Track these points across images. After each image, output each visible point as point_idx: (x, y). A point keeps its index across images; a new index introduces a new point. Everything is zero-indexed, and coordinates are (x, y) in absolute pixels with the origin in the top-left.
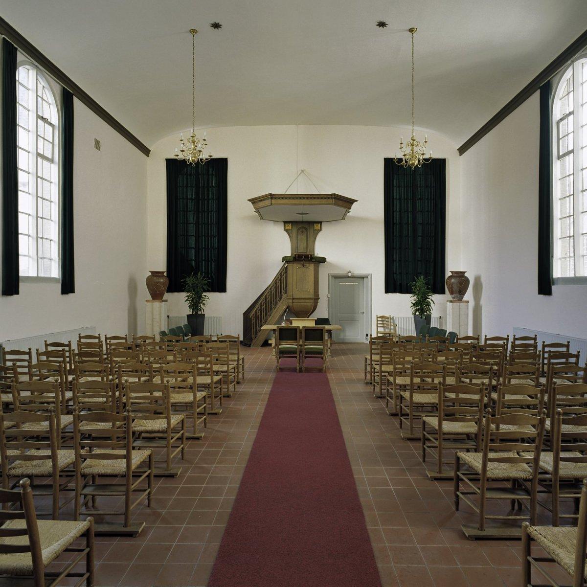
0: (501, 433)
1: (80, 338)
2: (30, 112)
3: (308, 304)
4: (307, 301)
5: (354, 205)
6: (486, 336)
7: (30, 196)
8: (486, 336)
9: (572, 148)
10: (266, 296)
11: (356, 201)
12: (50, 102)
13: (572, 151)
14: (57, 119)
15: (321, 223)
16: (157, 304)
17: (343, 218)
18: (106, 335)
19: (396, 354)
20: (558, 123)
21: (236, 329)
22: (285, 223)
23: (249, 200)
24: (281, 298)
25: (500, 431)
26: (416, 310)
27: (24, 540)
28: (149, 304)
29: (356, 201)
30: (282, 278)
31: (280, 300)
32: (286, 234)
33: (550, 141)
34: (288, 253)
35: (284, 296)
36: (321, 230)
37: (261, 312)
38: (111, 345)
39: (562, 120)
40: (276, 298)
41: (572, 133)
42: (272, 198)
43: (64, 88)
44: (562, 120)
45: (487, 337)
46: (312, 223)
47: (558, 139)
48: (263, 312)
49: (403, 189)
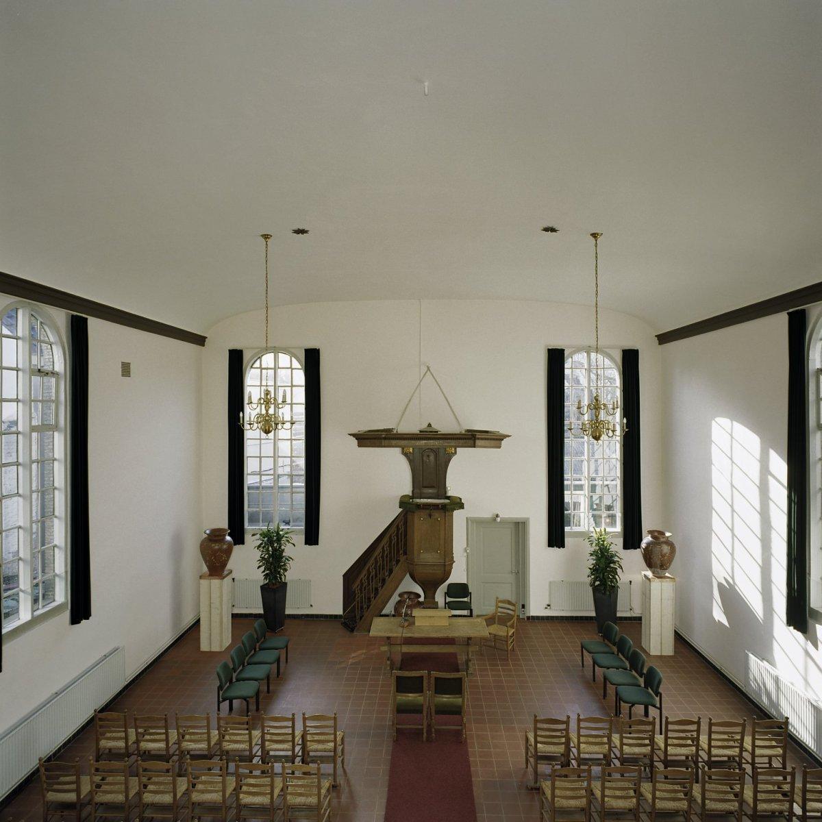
2: (19, 372)
7: (21, 500)
10: (376, 558)
12: (52, 339)
14: (63, 365)
16: (215, 582)
21: (331, 602)
23: (353, 435)
24: (398, 561)
26: (595, 580)
27: (74, 786)
28: (204, 582)
30: (379, 564)
31: (389, 576)
33: (806, 381)
35: (402, 558)
37: (369, 582)
40: (390, 562)
43: (5, 618)
45: (538, 718)
48: (401, 541)
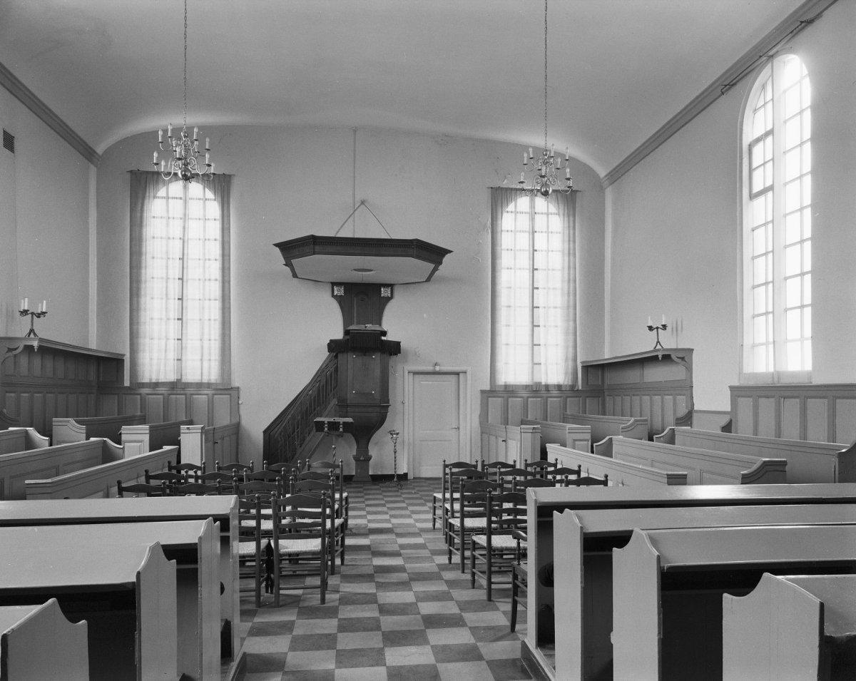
0: (329, 607)
1: (446, 466)
3: (372, 415)
4: (370, 409)
5: (448, 257)
6: (526, 461)
8: (526, 461)
9: (771, 183)
11: (450, 252)
13: (771, 188)
15: (391, 286)
17: (428, 280)
18: (444, 461)
19: (464, 485)
20: (750, 147)
22: (333, 284)
23: (276, 245)
25: (328, 605)
29: (450, 252)
32: (335, 306)
34: (339, 335)
36: (391, 298)
38: (452, 474)
39: (758, 140)
41: (771, 163)
42: (315, 243)
44: (758, 140)
46: (376, 287)
47: (751, 171)
49: (738, 251)
